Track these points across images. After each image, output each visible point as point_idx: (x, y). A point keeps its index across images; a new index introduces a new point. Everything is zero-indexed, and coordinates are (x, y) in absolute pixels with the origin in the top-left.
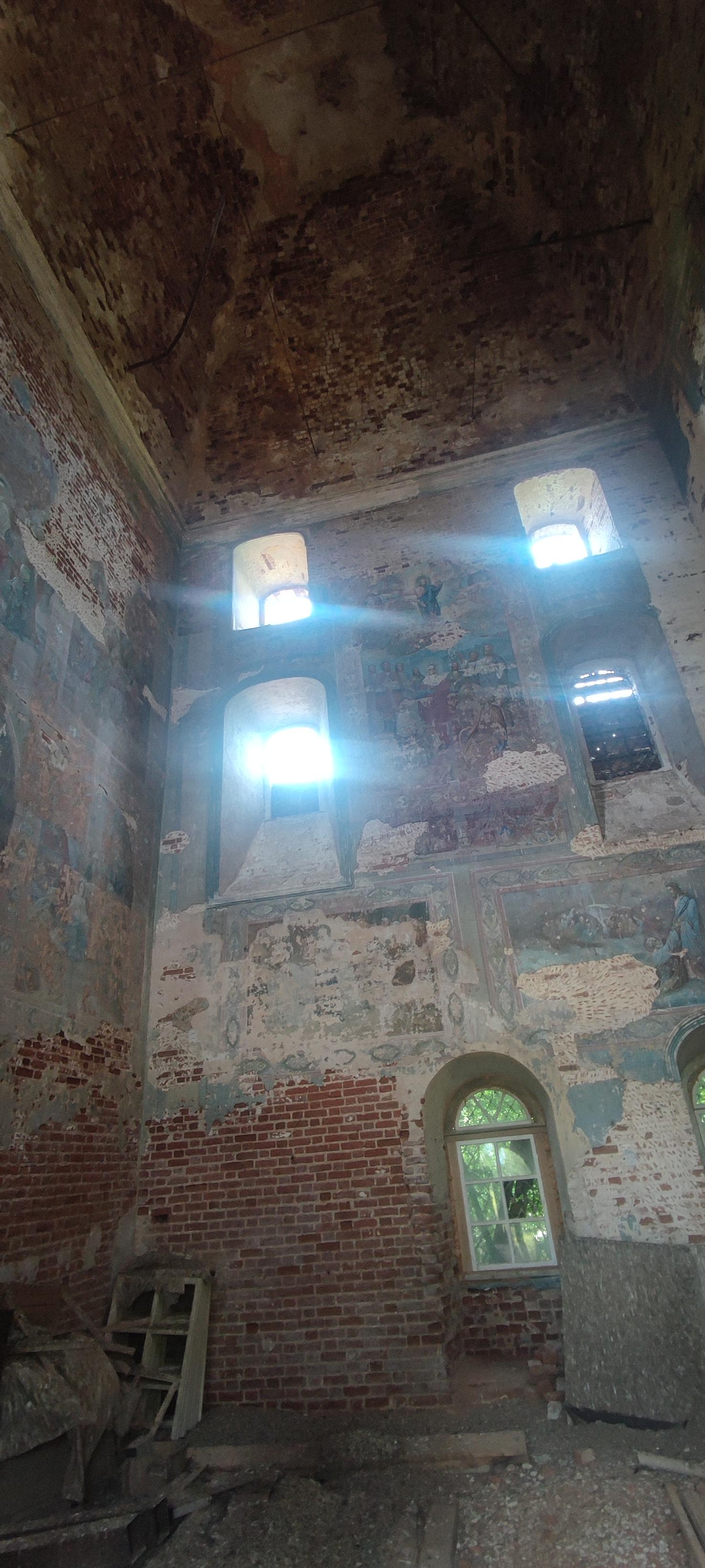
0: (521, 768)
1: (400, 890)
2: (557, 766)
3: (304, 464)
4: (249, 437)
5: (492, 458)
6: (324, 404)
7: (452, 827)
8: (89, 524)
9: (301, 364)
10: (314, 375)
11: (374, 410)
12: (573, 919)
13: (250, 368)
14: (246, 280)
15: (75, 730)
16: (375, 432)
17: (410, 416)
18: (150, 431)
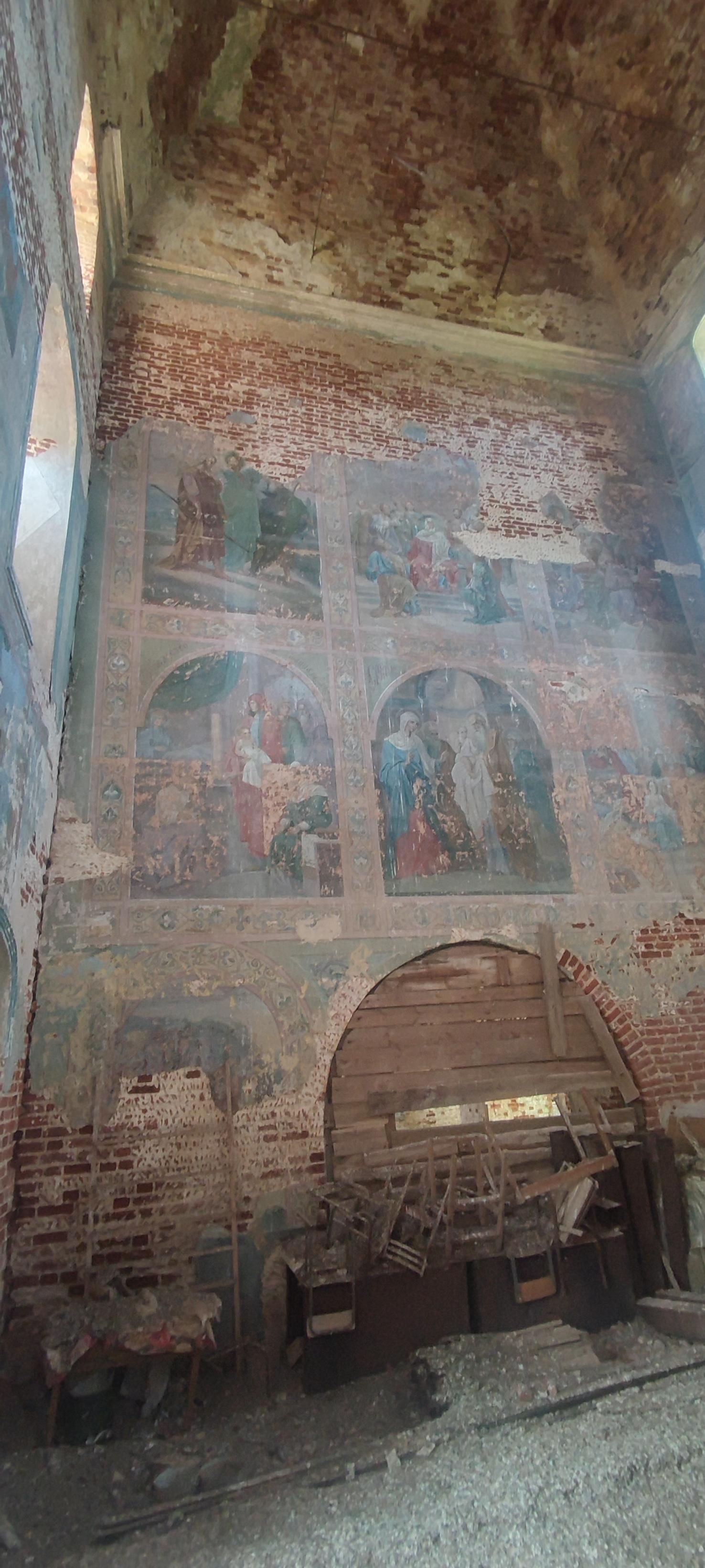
8: (524, 471)
14: (542, 72)
15: (585, 658)
18: (550, 318)
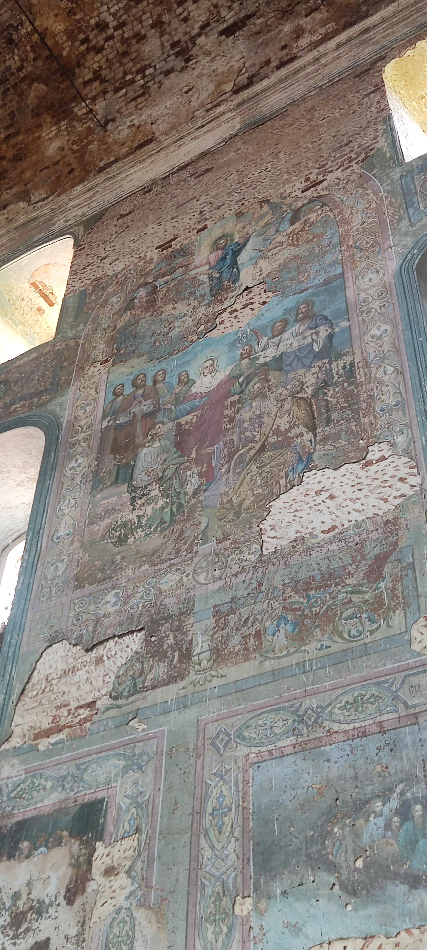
0: (332, 497)
1: (64, 778)
2: (402, 480)
3: (88, 144)
4: (17, 133)
5: (349, 40)
6: (110, 57)
7: (185, 634)
9: (75, 14)
10: (93, 22)
11: (179, 41)
12: (398, 812)
13: (10, 41)
16: (183, 69)
17: (229, 32)
